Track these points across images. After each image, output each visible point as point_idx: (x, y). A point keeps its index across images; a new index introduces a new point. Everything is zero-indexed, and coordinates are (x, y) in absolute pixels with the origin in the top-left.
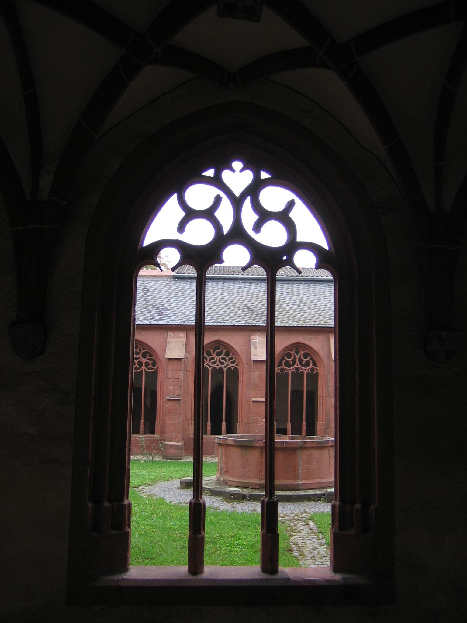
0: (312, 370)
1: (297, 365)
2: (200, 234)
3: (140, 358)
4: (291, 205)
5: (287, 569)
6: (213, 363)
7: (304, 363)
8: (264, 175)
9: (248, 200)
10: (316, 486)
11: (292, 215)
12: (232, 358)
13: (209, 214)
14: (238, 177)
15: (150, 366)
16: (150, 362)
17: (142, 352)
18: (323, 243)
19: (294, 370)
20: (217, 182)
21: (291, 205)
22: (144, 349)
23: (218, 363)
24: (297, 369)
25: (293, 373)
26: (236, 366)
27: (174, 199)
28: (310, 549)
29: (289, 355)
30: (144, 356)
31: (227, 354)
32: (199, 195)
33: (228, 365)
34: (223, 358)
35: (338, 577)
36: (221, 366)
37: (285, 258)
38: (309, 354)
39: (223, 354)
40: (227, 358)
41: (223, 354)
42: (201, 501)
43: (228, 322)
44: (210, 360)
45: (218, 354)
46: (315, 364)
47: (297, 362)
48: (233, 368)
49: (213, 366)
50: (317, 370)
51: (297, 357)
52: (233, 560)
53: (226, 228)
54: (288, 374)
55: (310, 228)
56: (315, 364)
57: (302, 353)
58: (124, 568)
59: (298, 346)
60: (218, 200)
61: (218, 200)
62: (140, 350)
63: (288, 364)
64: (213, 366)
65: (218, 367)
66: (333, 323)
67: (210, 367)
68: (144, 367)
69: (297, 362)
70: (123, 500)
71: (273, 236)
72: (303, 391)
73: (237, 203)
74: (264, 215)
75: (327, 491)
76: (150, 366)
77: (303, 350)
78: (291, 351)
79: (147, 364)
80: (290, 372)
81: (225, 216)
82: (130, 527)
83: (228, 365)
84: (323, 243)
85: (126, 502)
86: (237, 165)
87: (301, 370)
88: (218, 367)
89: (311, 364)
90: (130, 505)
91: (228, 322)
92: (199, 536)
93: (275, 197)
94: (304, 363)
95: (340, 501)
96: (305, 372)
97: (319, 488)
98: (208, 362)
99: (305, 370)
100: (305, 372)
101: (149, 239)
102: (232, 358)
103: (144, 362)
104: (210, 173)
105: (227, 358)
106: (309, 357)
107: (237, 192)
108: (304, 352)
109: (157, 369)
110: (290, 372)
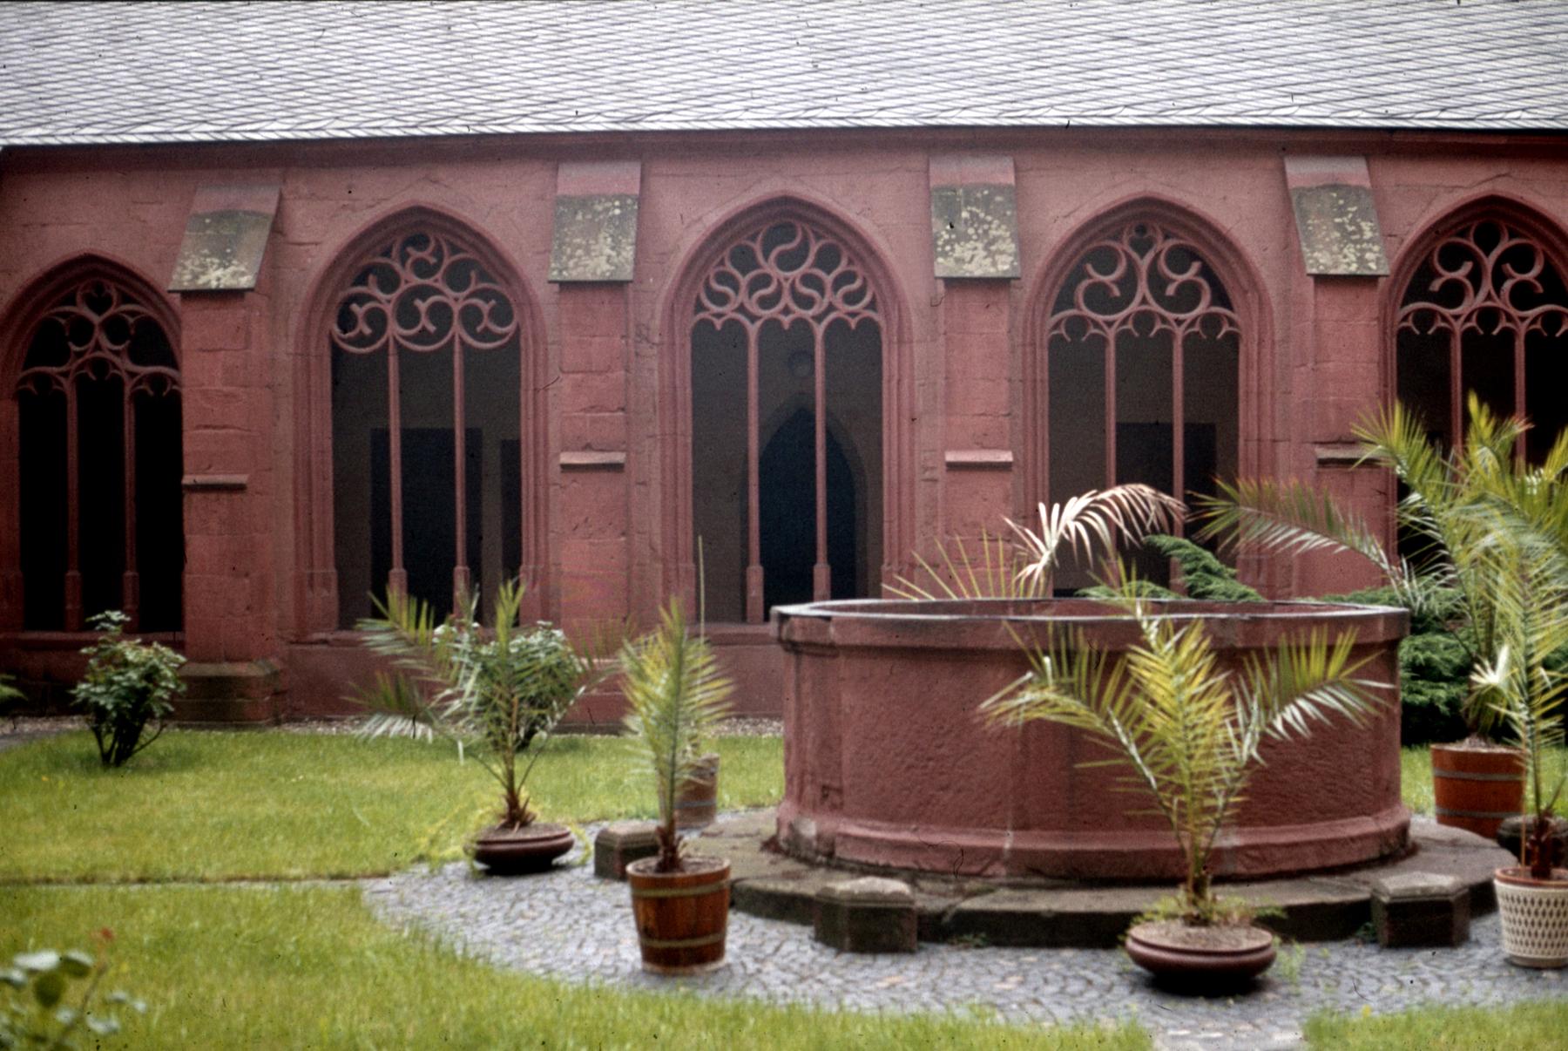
0: (1211, 322)
3: (438, 292)
6: (766, 303)
7: (1171, 290)
10: (1312, 863)
12: (848, 277)
15: (487, 322)
16: (485, 307)
19: (1129, 326)
22: (455, 250)
23: (786, 300)
24: (1144, 319)
25: (1123, 337)
29: (1106, 260)
30: (457, 279)
34: (808, 280)
39: (810, 259)
40: (828, 279)
41: (810, 259)
43: (826, 113)
46: (1221, 297)
47: (1143, 289)
48: (853, 323)
50: (1232, 323)
54: (1103, 341)
56: (1221, 297)
57: (1163, 245)
59: (1145, 217)
62: (438, 253)
63: (1101, 299)
65: (786, 320)
67: (753, 319)
68: (457, 329)
69: (1143, 289)
78: (1117, 238)
79: (471, 317)
88: (786, 320)
89: (1206, 297)
91: (826, 113)
94: (1171, 290)
96: (1180, 332)
98: (742, 297)
99: (1181, 324)
100: (1180, 332)
102: (848, 277)
105: (828, 279)
106: (1196, 266)
108: (1172, 242)
110: (1111, 334)
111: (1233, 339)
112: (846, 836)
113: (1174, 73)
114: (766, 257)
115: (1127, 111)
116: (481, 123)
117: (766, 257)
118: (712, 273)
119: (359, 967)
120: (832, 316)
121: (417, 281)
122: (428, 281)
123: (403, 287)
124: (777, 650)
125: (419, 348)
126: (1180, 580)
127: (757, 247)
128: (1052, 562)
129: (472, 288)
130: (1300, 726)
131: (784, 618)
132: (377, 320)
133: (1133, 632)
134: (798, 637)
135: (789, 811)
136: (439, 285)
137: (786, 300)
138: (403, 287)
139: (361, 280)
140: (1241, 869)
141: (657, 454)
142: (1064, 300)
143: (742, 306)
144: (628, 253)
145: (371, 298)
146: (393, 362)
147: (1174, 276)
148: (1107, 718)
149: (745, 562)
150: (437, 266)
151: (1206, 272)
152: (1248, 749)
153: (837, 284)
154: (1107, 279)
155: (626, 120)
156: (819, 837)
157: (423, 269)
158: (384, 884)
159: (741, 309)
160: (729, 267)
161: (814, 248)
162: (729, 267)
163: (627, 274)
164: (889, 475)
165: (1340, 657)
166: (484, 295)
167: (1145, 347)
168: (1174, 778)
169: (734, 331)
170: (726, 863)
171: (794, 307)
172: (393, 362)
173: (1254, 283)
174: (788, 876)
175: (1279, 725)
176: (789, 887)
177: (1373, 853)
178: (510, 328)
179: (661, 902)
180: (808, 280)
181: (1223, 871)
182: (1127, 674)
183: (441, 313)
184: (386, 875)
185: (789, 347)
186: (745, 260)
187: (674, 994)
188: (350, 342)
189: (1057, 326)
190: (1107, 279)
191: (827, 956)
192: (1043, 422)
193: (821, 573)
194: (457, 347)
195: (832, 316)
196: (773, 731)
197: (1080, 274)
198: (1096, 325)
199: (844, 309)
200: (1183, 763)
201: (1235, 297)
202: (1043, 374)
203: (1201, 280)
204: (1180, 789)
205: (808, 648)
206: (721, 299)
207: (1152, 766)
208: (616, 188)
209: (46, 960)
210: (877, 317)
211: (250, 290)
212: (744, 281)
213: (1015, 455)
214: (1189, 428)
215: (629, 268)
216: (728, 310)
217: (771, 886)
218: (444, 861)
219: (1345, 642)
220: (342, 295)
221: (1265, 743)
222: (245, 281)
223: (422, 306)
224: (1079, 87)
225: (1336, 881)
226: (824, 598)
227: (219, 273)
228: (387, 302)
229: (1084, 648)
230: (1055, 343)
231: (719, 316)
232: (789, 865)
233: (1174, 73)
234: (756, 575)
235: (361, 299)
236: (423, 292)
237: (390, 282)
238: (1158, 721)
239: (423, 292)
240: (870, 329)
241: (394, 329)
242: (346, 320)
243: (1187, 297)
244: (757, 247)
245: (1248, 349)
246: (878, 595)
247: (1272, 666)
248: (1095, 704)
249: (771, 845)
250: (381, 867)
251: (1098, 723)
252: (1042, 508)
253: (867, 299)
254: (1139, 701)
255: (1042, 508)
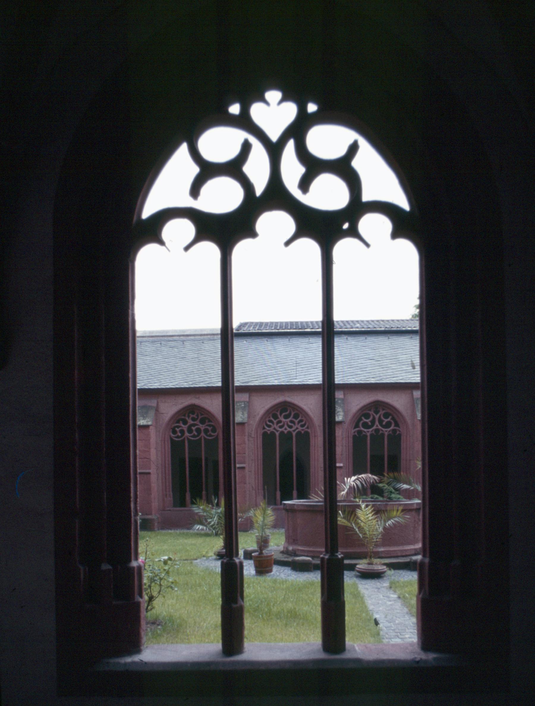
0: (394, 431)
1: (377, 426)
2: (222, 197)
3: (197, 425)
4: (353, 148)
5: (358, 645)
6: (281, 427)
7: (384, 423)
8: (312, 108)
9: (290, 146)
10: (399, 554)
11: (356, 163)
12: (301, 421)
13: (234, 168)
14: (274, 113)
15: (210, 432)
16: (210, 428)
17: (200, 417)
18: (404, 204)
19: (373, 432)
20: (245, 122)
21: (353, 148)
22: (202, 415)
23: (286, 426)
24: (377, 430)
25: (372, 435)
26: (307, 430)
27: (183, 149)
28: (388, 618)
29: (367, 416)
30: (202, 422)
31: (296, 416)
32: (219, 142)
33: (297, 428)
34: (291, 422)
35: (431, 656)
36: (289, 429)
37: (346, 226)
38: (390, 411)
39: (292, 416)
40: (296, 421)
41: (292, 416)
42: (237, 561)
43: (296, 380)
44: (277, 424)
45: (286, 417)
46: (397, 424)
47: (377, 423)
48: (303, 432)
49: (280, 430)
50: (400, 431)
51: (377, 417)
52: (280, 635)
53: (259, 189)
54: (366, 436)
55: (381, 180)
56: (397, 424)
57: (382, 412)
58: (135, 646)
59: (377, 405)
60: (246, 147)
61: (246, 147)
62: (197, 415)
63: (365, 425)
64: (280, 430)
65: (286, 432)
66: (419, 378)
67: (277, 431)
68: (203, 434)
69: (377, 423)
70: (130, 561)
71: (328, 194)
72: (384, 456)
73: (275, 151)
74: (313, 167)
75: (411, 559)
76: (210, 432)
77: (383, 410)
78: (370, 410)
79: (206, 431)
80: (368, 434)
81: (258, 170)
82: (141, 596)
83: (297, 428)
84: (404, 204)
85: (134, 564)
86: (273, 96)
87: (381, 432)
88: (286, 432)
89: (393, 425)
90: (140, 568)
91: (296, 380)
92: (234, 606)
93: (329, 140)
94: (384, 423)
95: (431, 557)
96: (386, 434)
97: (403, 556)
98: (275, 426)
99: (386, 431)
100: (386, 434)
101: (150, 208)
102: (301, 421)
103: (202, 429)
104: (235, 109)
105: (296, 421)
106: (390, 417)
107: (274, 136)
108: (384, 411)
109: (217, 436)
110: (368, 434)
111: (400, 435)
112: (298, 550)
113: (385, 369)
114: (281, 415)
115: (372, 379)
116: (208, 384)
117: (281, 415)
118: (267, 419)
119: (197, 574)
120: (297, 430)
121: (192, 422)
122: (195, 422)
123: (189, 424)
124: (284, 511)
125: (192, 439)
126: (386, 494)
127: (278, 414)
128: (347, 491)
129: (206, 424)
130: (392, 525)
131: (285, 504)
132: (182, 432)
133: (359, 507)
134: (288, 508)
135: (286, 545)
136: (198, 423)
137: (286, 426)
138: (189, 424)
139: (178, 422)
140: (383, 555)
141: (253, 465)
142: (357, 426)
143: (275, 428)
144: (246, 415)
145: (180, 427)
146: (186, 442)
147: (384, 419)
148: (351, 524)
149: (276, 490)
150: (197, 418)
151: (393, 418)
152: (381, 529)
153: (299, 422)
154: (367, 421)
155: (245, 383)
156: (293, 550)
157: (193, 419)
158: (196, 561)
159: (275, 429)
160: (272, 419)
161: (293, 414)
162: (272, 419)
163: (246, 420)
164: (312, 470)
165: (400, 511)
166: (210, 426)
167: (377, 437)
168: (366, 536)
169: (273, 434)
170: (273, 553)
171: (287, 428)
172: (186, 442)
173: (405, 421)
174: (285, 558)
175: (387, 525)
176: (286, 559)
177: (413, 552)
178: (216, 434)
179: (259, 561)
180: (291, 422)
181: (378, 555)
182: (355, 515)
183: (198, 430)
184: (196, 559)
185: (286, 438)
186: (275, 417)
187: (261, 578)
188: (176, 437)
189: (354, 432)
190: (367, 421)
191: (294, 572)
192: (351, 455)
193: (295, 493)
194: (203, 438)
195: (297, 430)
196: (283, 531)
197: (360, 419)
198: (365, 432)
199: (300, 429)
200: (367, 532)
201: (400, 425)
202: (351, 444)
203: (392, 421)
204: (367, 538)
205: (291, 510)
206: (269, 426)
207: (361, 533)
208: (242, 399)
209: (166, 558)
210: (309, 431)
211: (151, 425)
212: (275, 422)
213: (343, 464)
214: (389, 456)
215: (246, 419)
216: (271, 429)
217: (282, 559)
218: (209, 557)
219: (401, 508)
220: (173, 426)
221: (385, 528)
222: (150, 423)
223: (194, 428)
224: (360, 373)
225: (405, 558)
226: (296, 499)
227: (143, 421)
228: (185, 427)
229: (347, 510)
230: (354, 437)
231: (269, 430)
232: (285, 556)
233: (385, 369)
234: (278, 493)
235: (178, 427)
236: (194, 425)
237: (185, 422)
238: (362, 524)
239: (194, 425)
240: (307, 434)
241: (187, 434)
242: (174, 432)
243: (388, 425)
244: (278, 414)
245: (403, 438)
246: (310, 499)
247: (386, 513)
248: (349, 521)
249: (282, 552)
250: (195, 558)
251: (349, 525)
252: (346, 479)
253: (306, 427)
254: (358, 520)
255: (346, 479)
